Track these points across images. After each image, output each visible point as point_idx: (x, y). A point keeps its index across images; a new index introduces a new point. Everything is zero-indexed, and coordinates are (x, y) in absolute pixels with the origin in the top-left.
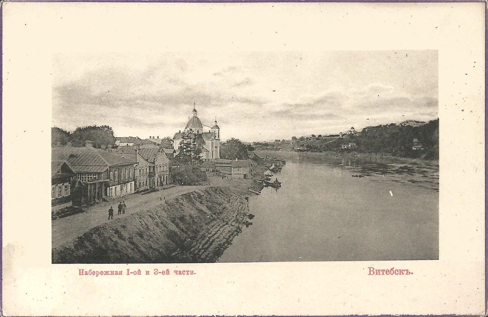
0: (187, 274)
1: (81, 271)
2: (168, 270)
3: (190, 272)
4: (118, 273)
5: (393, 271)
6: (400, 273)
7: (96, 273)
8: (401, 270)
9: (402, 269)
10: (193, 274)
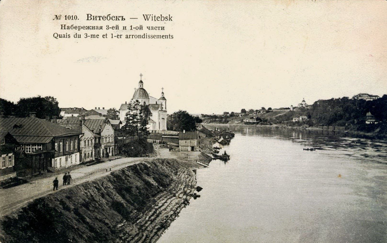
0: (122, 20)
3: (161, 28)
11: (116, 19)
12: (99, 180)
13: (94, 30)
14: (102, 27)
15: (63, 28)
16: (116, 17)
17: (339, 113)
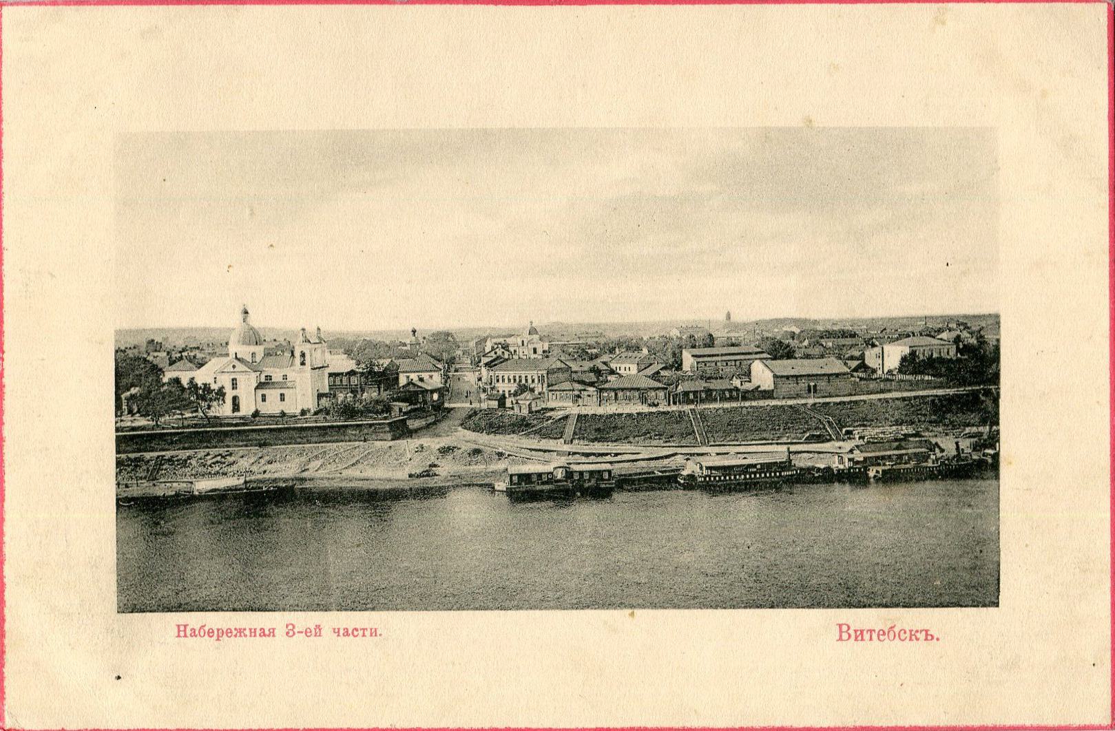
0: (926, 639)
1: (182, 628)
3: (369, 630)
4: (267, 632)
5: (204, 630)
6: (911, 637)
11: (908, 638)
14: (274, 629)
15: (182, 634)
16: (911, 631)
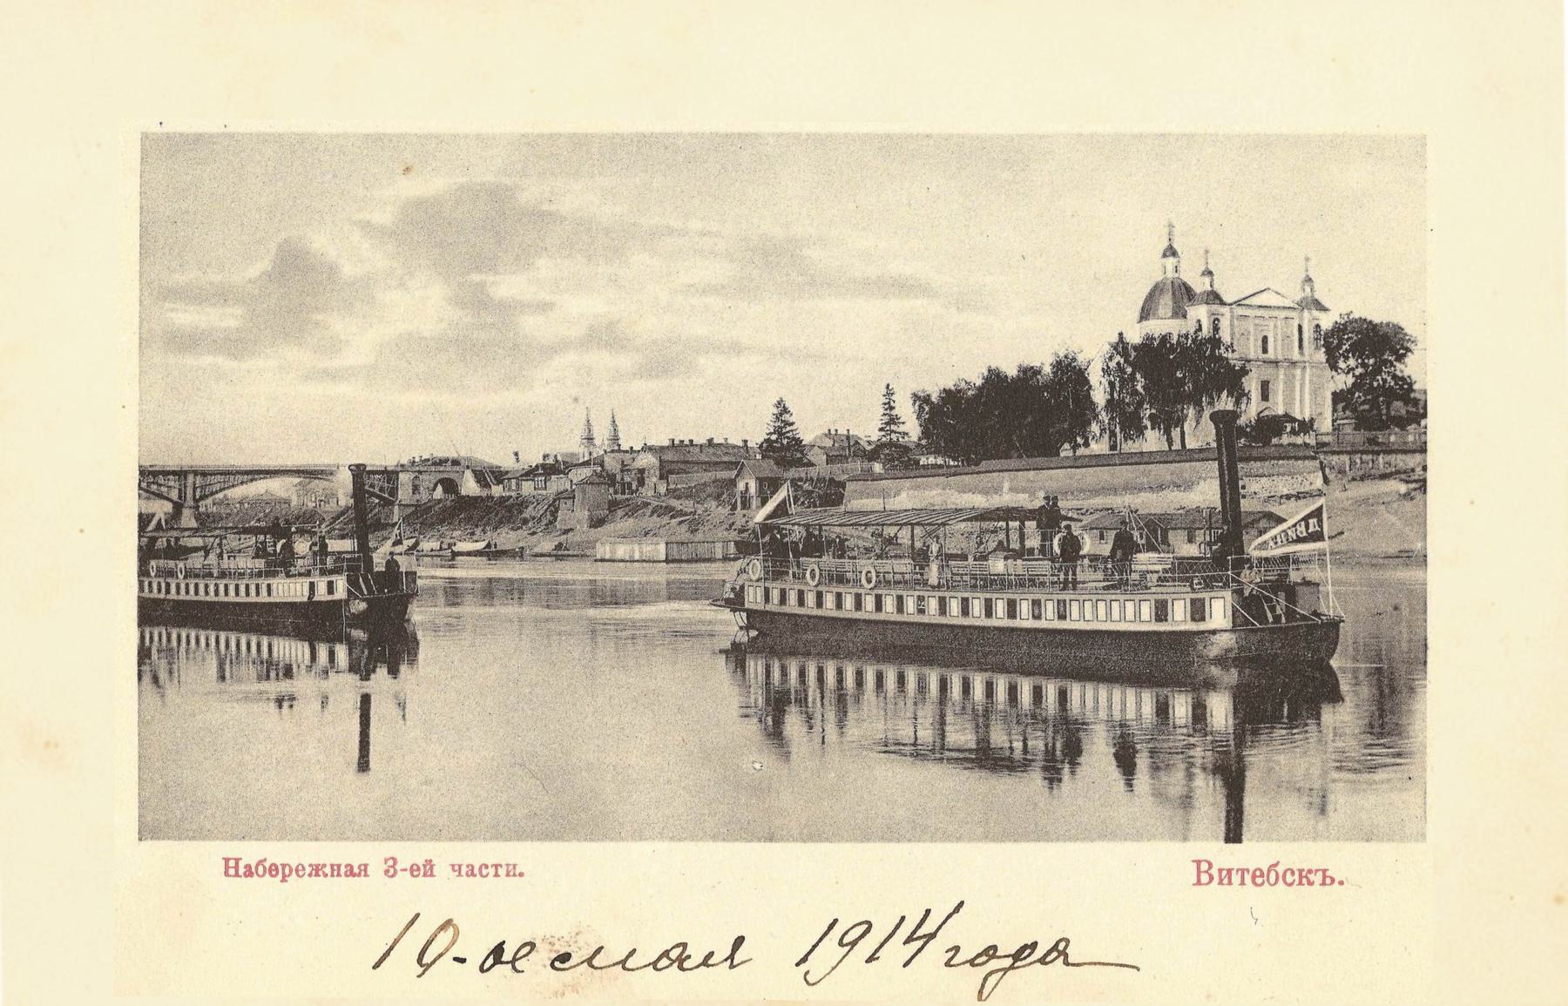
0: (1324, 884)
2: (431, 861)
3: (505, 867)
4: (356, 870)
7: (280, 868)
8: (1303, 870)
9: (1306, 868)
10: (514, 875)
11: (1297, 882)
12: (493, 472)
13: (339, 878)
14: (366, 865)
17: (490, 320)
